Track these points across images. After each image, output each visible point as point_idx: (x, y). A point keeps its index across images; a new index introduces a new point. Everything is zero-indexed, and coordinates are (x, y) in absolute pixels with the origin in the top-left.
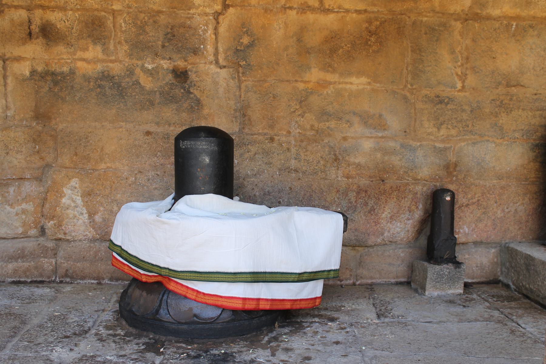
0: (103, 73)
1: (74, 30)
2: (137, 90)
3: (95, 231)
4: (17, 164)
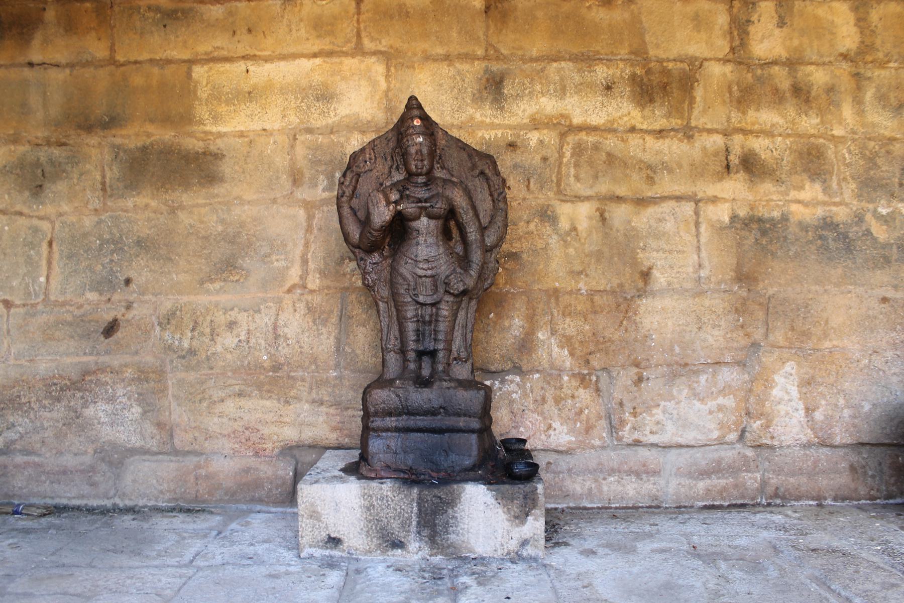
0: (824, 219)
1: (785, 162)
2: (868, 242)
3: (814, 433)
4: (714, 343)
